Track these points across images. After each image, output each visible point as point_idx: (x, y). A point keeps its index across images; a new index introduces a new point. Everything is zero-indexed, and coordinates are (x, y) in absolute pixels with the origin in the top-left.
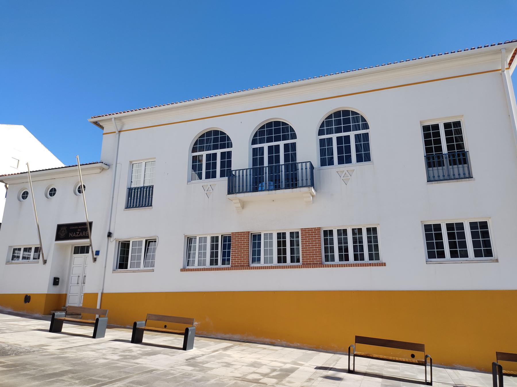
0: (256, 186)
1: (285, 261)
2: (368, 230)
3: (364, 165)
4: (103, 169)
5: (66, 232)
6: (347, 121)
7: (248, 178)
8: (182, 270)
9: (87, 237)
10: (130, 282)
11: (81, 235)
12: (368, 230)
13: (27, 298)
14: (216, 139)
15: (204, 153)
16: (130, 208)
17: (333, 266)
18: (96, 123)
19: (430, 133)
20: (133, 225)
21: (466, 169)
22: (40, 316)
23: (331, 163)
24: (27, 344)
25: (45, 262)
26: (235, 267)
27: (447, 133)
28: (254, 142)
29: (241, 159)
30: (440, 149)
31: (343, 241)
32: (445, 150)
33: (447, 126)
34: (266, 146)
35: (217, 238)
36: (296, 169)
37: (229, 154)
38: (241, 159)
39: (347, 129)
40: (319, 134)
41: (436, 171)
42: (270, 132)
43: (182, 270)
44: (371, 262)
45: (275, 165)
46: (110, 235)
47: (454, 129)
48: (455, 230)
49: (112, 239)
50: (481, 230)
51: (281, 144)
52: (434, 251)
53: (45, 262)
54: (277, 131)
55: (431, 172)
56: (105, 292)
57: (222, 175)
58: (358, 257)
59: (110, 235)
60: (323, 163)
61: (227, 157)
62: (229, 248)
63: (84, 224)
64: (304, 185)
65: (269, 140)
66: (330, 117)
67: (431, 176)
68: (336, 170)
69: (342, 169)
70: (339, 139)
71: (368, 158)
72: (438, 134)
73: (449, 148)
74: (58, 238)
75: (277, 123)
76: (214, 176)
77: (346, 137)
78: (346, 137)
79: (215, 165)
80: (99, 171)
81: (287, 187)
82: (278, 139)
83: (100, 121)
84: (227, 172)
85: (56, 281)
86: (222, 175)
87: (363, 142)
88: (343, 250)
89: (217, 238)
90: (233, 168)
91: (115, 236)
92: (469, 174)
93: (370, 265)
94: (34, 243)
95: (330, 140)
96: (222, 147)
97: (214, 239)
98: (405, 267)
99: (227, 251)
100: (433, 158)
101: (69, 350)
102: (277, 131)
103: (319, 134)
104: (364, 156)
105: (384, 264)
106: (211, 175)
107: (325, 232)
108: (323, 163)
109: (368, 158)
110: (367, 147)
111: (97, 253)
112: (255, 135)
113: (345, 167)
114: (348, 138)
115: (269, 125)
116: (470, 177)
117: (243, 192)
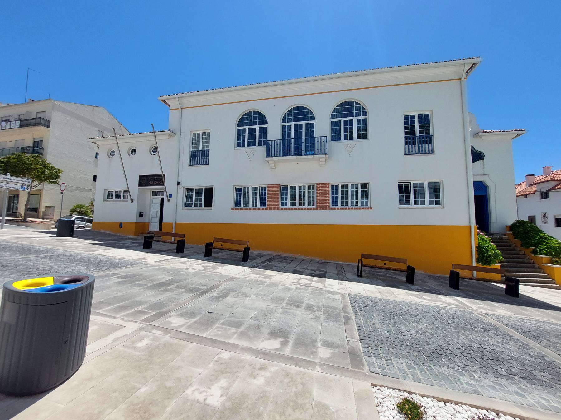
0: (286, 152)
1: (295, 205)
2: (342, 186)
3: (362, 141)
4: (170, 136)
5: (145, 180)
6: (351, 109)
7: (279, 147)
8: (232, 209)
9: (163, 184)
10: (198, 215)
11: (152, 183)
12: (342, 186)
13: (121, 225)
14: (255, 118)
15: (247, 128)
16: (193, 165)
17: (337, 209)
18: (164, 101)
19: (409, 121)
20: (198, 178)
21: (414, 148)
22: (91, 238)
23: (339, 139)
24: (131, 258)
25: (132, 201)
26: (269, 208)
27: (420, 122)
28: (239, 125)
29: (274, 132)
30: (414, 133)
31: (302, 193)
32: (417, 134)
33: (420, 116)
34: (292, 124)
35: (257, 188)
36: (314, 142)
37: (265, 129)
38: (274, 132)
39: (351, 115)
40: (283, 122)
41: (411, 148)
42: (295, 114)
43: (232, 209)
44: (261, 207)
45: (298, 139)
46: (178, 183)
47: (425, 119)
48: (419, 188)
49: (180, 186)
50: (209, 192)
51: (257, 127)
52: (188, 203)
53: (132, 201)
54: (255, 118)
55: (407, 148)
56: (177, 222)
57: (260, 144)
58: (345, 203)
59: (178, 183)
60: (333, 139)
61: (263, 131)
62: (265, 195)
63: (160, 175)
64: (322, 152)
65: (295, 120)
66: (340, 105)
67: (407, 151)
68: (343, 144)
69: (347, 143)
70: (345, 122)
71: (365, 137)
72: (413, 122)
73: (421, 132)
74: (140, 185)
75: (301, 108)
76: (254, 144)
77: (351, 121)
78: (351, 121)
79: (254, 136)
80: (167, 137)
81: (295, 155)
82: (301, 120)
83: (167, 99)
84: (264, 141)
85: (141, 214)
86: (260, 144)
87: (363, 124)
88: (293, 198)
89: (257, 188)
90: (268, 139)
91: (182, 184)
92: (432, 150)
93: (362, 208)
94: (122, 187)
95: (339, 122)
96: (260, 123)
97: (255, 189)
98: (385, 211)
99: (264, 197)
100: (409, 139)
101: (164, 262)
102: (301, 114)
103: (283, 122)
104: (362, 135)
105: (371, 208)
106: (252, 143)
107: (333, 187)
108: (333, 139)
109: (365, 137)
110: (365, 129)
111: (170, 196)
112: (240, 120)
113: (349, 142)
114: (351, 121)
115: (295, 109)
116: (433, 152)
117: (277, 156)
